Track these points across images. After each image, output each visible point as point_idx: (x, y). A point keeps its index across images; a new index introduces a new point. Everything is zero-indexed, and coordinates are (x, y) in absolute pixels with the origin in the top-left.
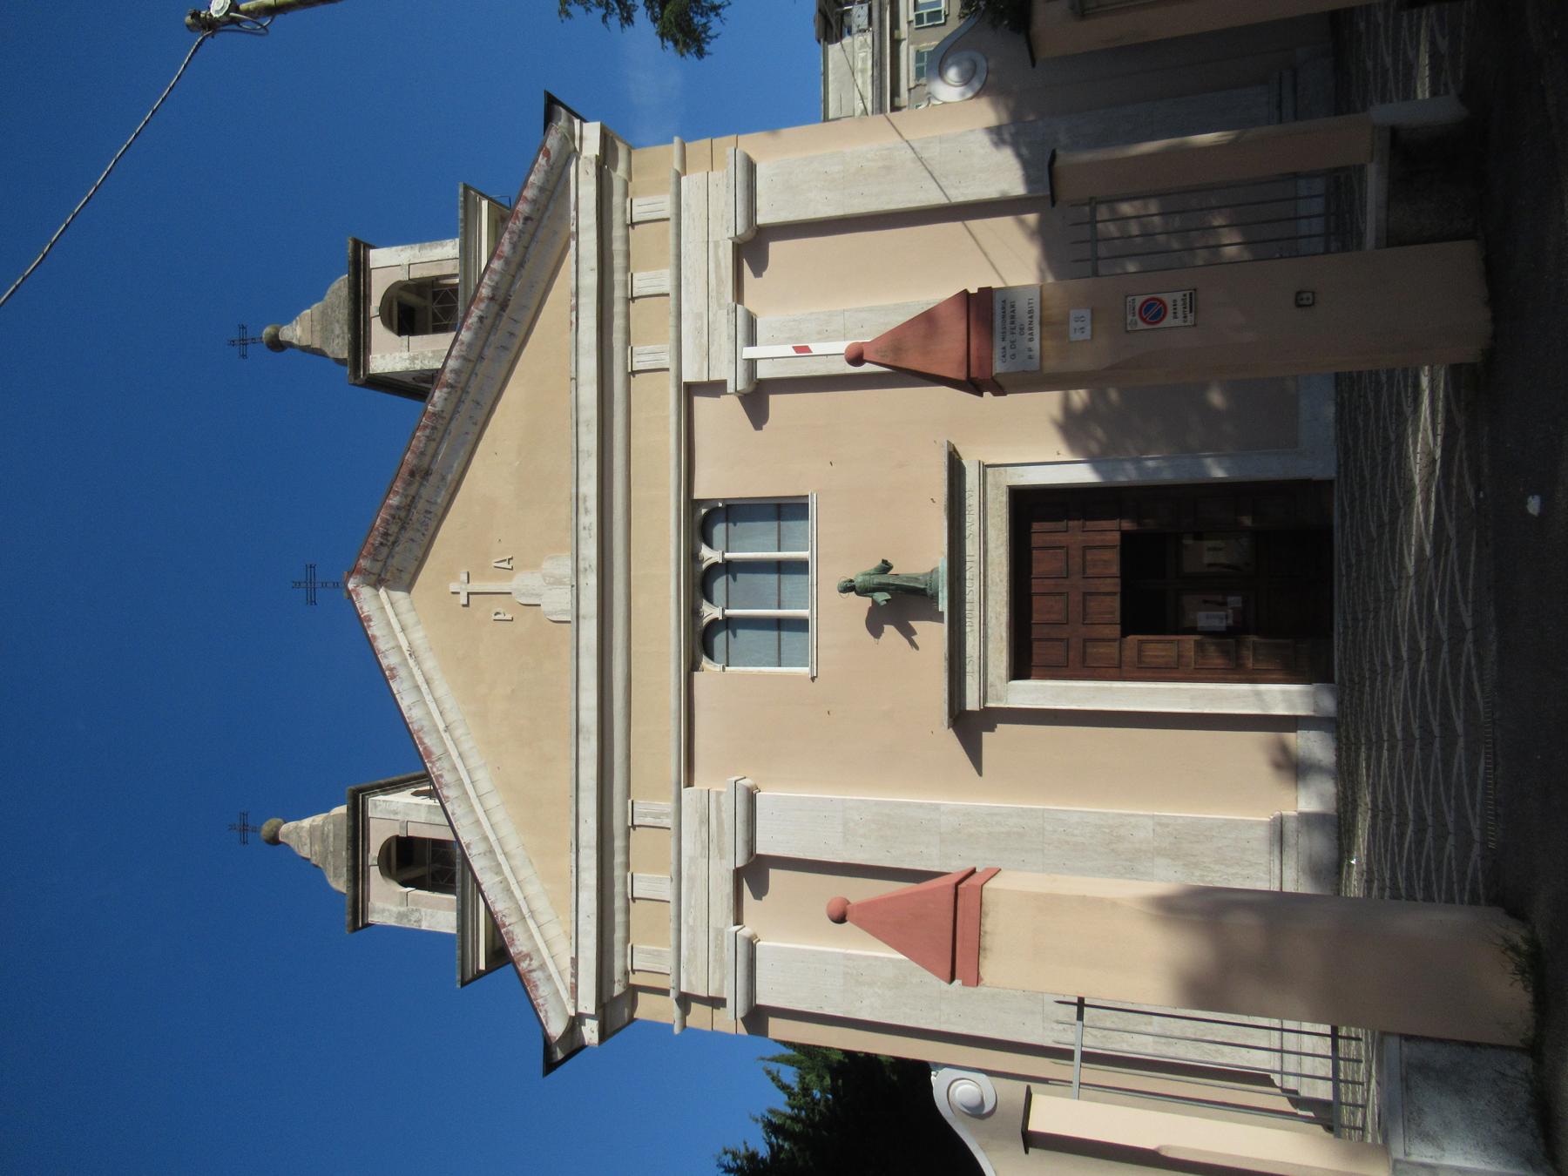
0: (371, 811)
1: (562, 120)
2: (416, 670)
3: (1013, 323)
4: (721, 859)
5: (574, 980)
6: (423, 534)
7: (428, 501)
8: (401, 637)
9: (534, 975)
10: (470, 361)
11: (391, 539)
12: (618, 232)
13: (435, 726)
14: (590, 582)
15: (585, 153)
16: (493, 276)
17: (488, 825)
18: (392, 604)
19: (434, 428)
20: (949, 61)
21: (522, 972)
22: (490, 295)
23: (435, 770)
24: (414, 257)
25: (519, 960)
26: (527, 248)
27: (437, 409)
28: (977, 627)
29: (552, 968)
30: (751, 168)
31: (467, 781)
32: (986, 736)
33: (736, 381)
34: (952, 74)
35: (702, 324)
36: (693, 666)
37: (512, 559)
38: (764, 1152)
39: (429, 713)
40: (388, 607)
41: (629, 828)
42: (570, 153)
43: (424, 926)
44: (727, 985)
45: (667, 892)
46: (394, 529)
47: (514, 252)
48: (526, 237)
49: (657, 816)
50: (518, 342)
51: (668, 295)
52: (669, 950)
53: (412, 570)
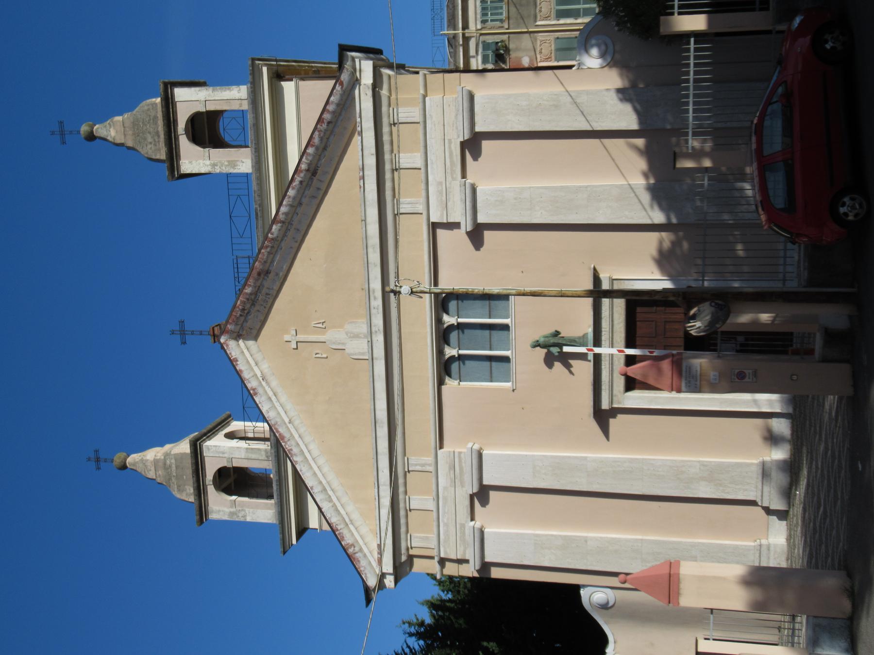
0: (206, 453)
1: (349, 61)
2: (267, 388)
3: (690, 374)
4: (462, 487)
5: (379, 556)
6: (265, 307)
7: (267, 288)
8: (256, 369)
9: (357, 555)
10: (294, 206)
11: (246, 312)
12: (386, 129)
13: (283, 420)
14: (379, 339)
15: (363, 81)
16: (308, 157)
17: (321, 475)
18: (248, 349)
19: (272, 247)
20: (593, 42)
21: (350, 554)
22: (307, 168)
23: (287, 446)
24: (209, 95)
25: (348, 548)
26: (328, 139)
27: (274, 236)
28: (608, 366)
29: (365, 550)
30: (471, 97)
31: (305, 451)
32: (612, 421)
33: (467, 225)
34: (595, 51)
35: (442, 189)
36: (441, 383)
37: (325, 322)
38: (428, 620)
39: (279, 413)
40: (245, 351)
41: (406, 472)
42: (355, 81)
43: (249, 519)
44: (471, 553)
45: (431, 506)
46: (248, 306)
47: (321, 143)
48: (328, 133)
49: (423, 465)
50: (322, 192)
51: (420, 169)
52: (434, 536)
53: (258, 327)
